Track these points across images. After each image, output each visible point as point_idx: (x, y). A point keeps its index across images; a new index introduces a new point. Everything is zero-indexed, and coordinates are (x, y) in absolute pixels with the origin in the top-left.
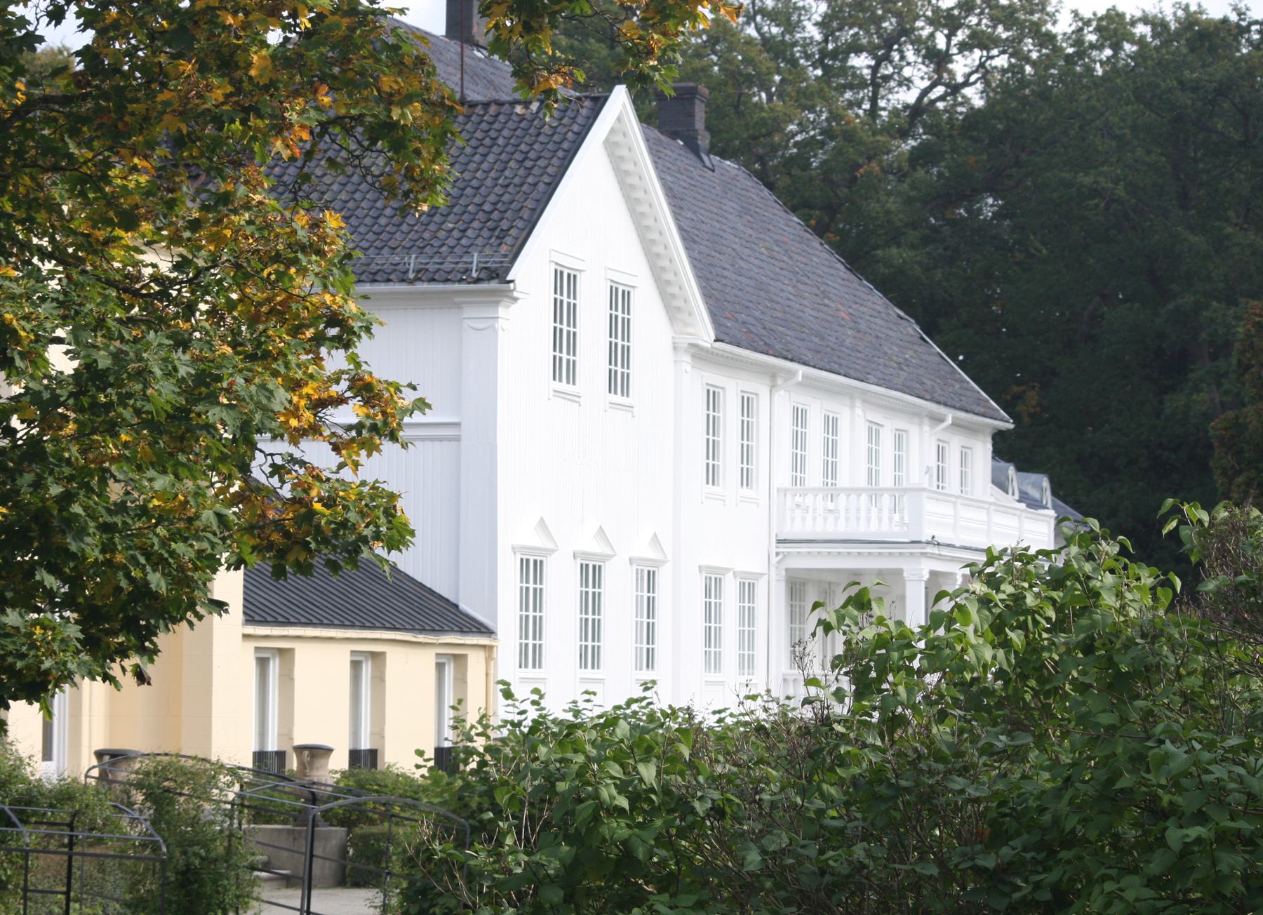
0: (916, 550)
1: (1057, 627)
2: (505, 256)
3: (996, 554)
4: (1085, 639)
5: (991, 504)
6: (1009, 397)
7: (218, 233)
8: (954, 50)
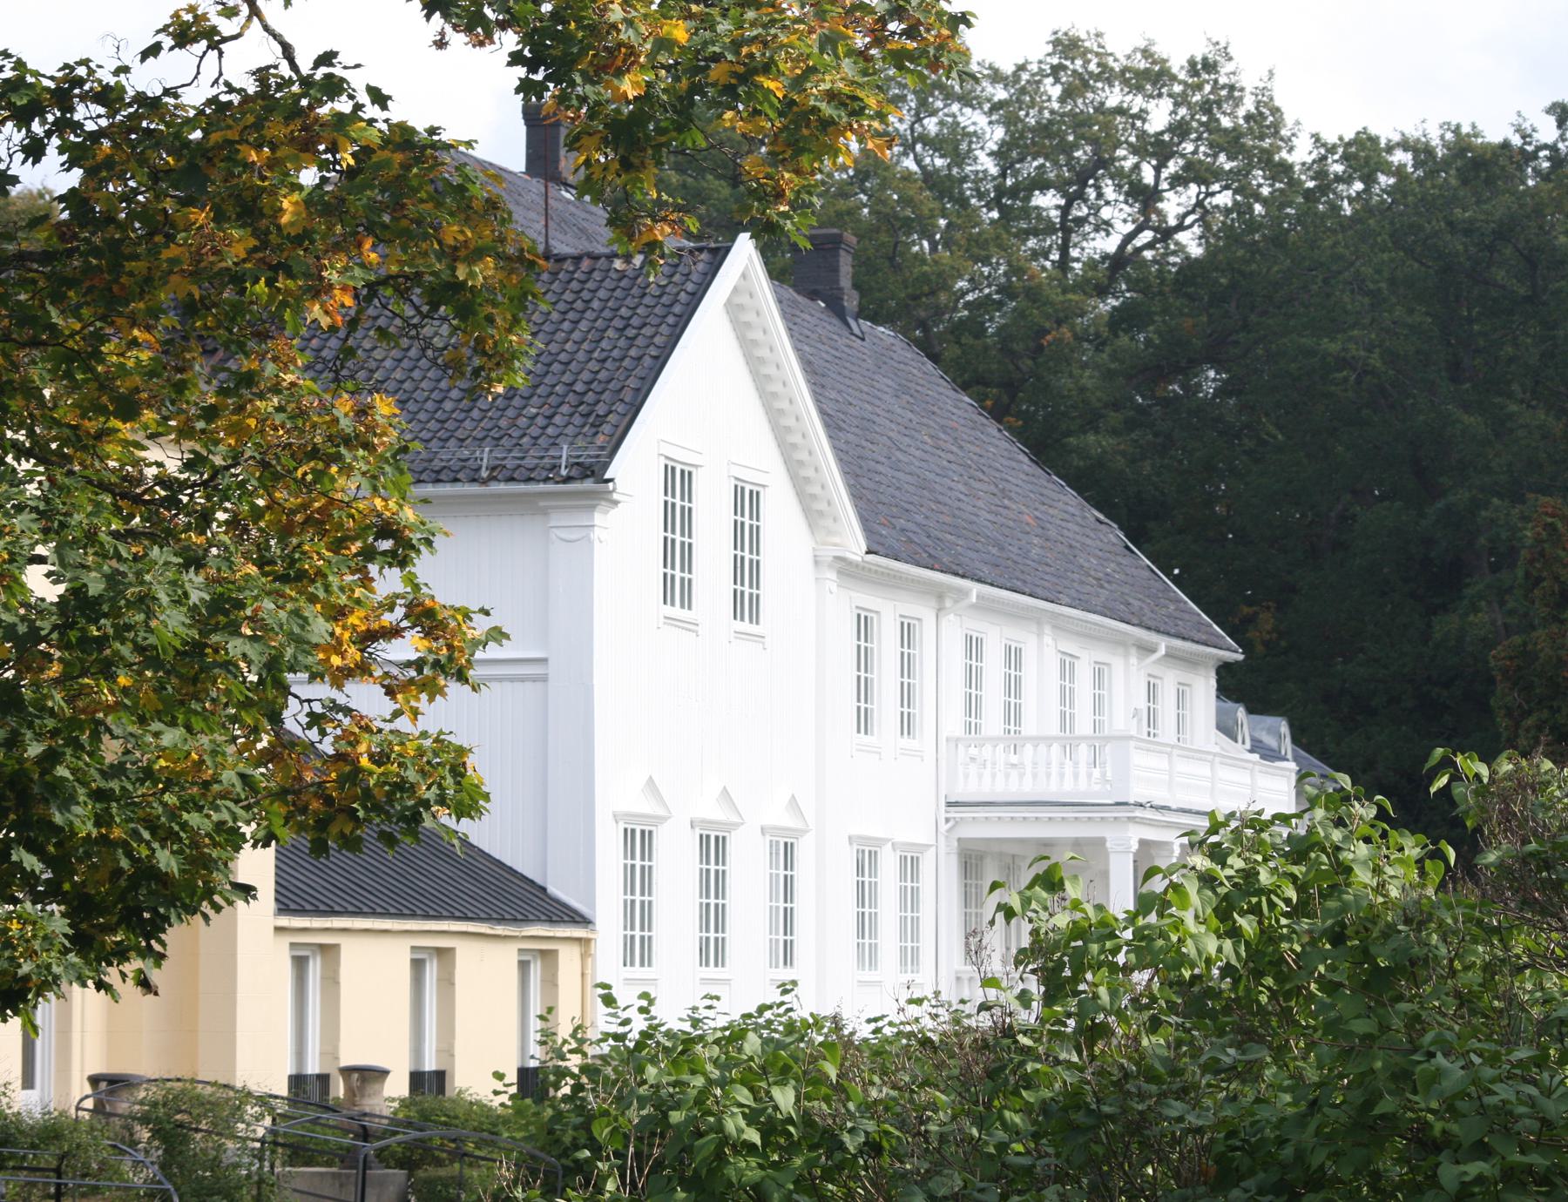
0: (1122, 813)
1: (1299, 910)
2: (602, 448)
3: (1221, 819)
4: (1333, 926)
5: (1215, 755)
6: (1237, 621)
7: (239, 423)
8: (1164, 186)
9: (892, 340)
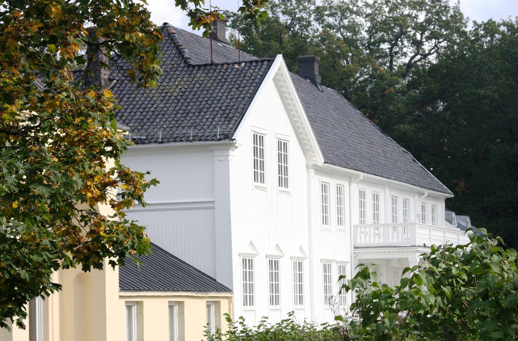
0: (414, 249)
1: (467, 284)
2: (231, 129)
3: (436, 248)
4: (483, 291)
5: (445, 229)
6: (452, 185)
7: (52, 103)
8: (424, 40)
9: (333, 92)
